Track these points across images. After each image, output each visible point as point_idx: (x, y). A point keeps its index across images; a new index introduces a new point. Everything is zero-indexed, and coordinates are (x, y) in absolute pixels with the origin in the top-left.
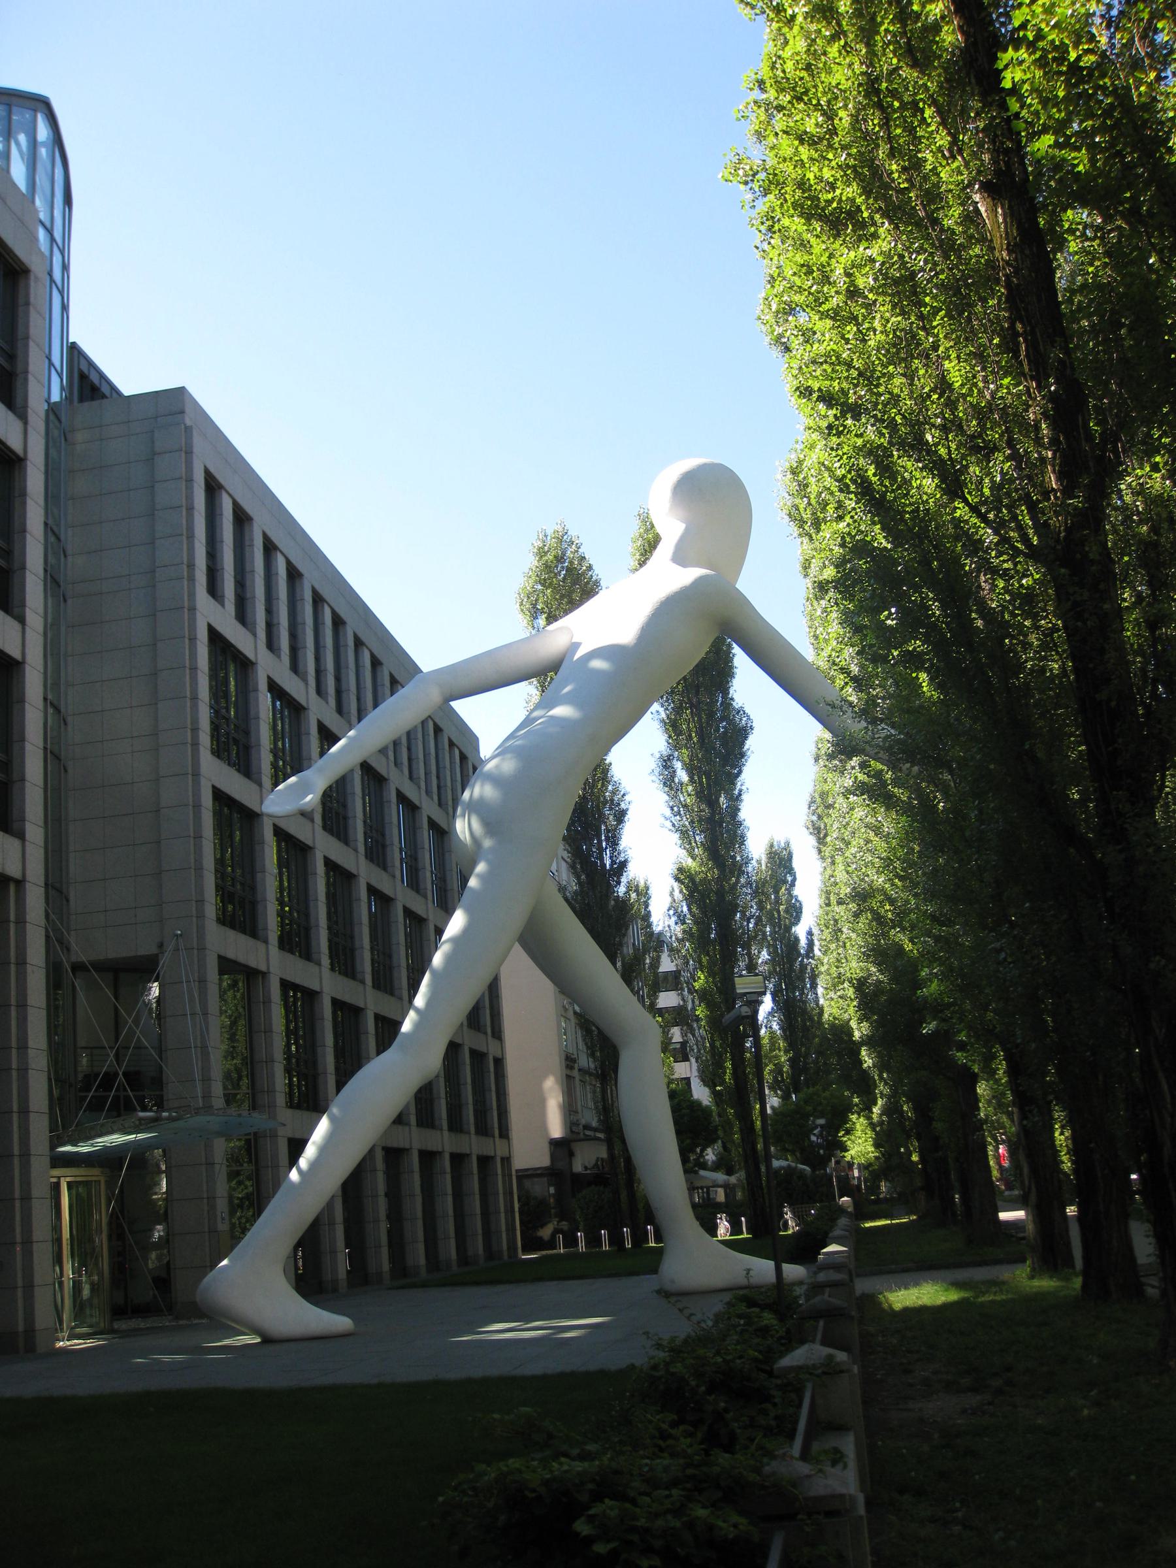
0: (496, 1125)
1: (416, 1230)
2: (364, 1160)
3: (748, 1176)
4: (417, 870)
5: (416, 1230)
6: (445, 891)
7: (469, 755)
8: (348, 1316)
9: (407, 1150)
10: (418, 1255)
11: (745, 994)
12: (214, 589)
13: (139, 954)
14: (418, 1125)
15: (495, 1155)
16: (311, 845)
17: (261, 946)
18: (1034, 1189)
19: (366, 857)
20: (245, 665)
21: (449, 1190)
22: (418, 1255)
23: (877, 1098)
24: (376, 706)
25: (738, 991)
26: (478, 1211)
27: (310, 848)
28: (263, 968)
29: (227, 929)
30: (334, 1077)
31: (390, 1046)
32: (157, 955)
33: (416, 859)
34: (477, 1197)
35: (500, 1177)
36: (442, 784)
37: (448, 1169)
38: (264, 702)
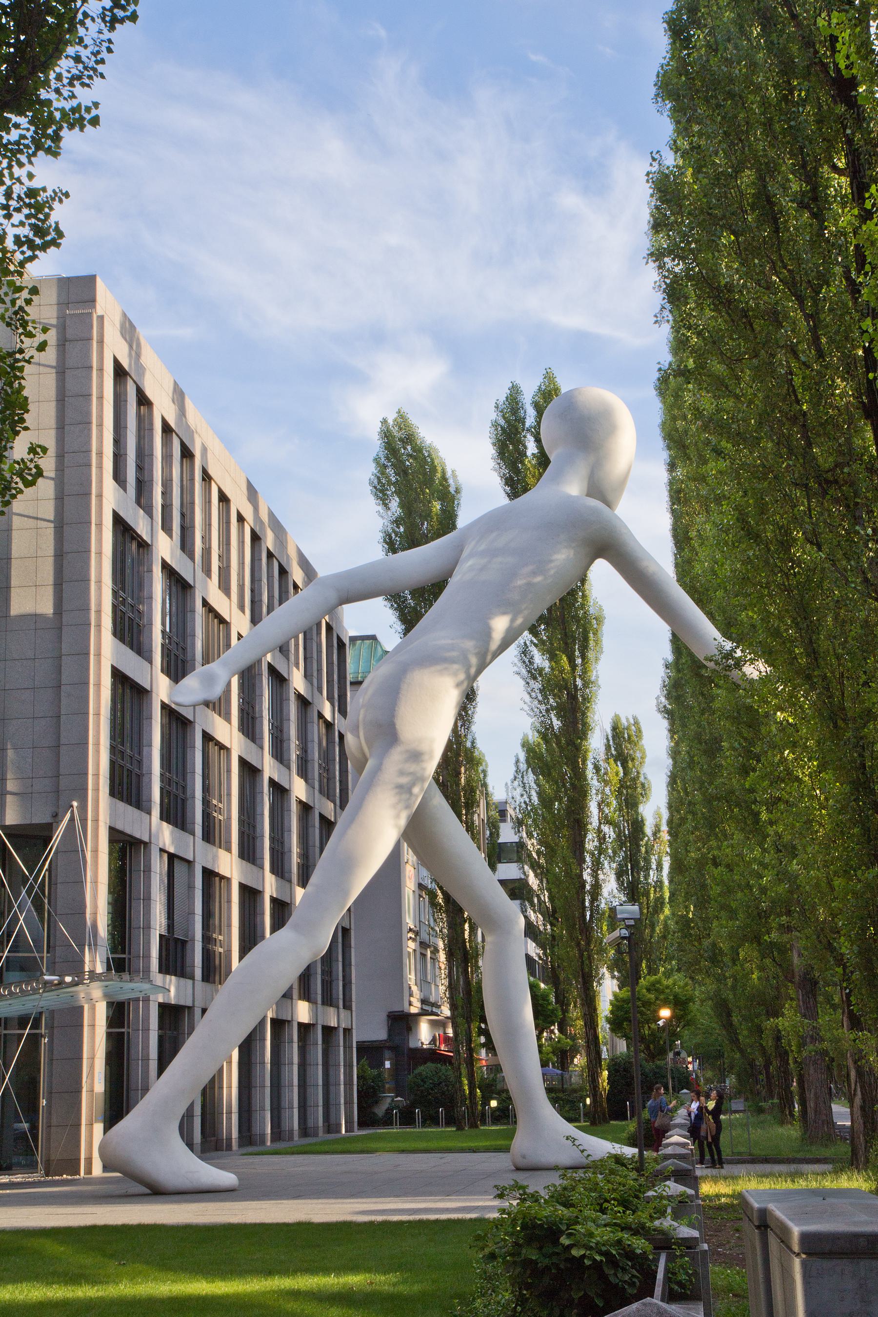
0: (341, 996)
1: (264, 1097)
2: (255, 1029)
3: (590, 1061)
4: (282, 741)
5: (264, 1097)
6: (306, 761)
7: (334, 626)
8: (235, 1173)
9: (289, 1021)
10: (231, 1125)
11: (624, 920)
12: (119, 477)
13: (33, 822)
14: (203, 980)
15: (339, 1027)
16: (149, 689)
17: (145, 816)
18: (859, 1089)
19: (115, 634)
20: (144, 546)
21: (296, 1060)
22: (231, 1125)
23: (727, 635)
24: (280, 604)
25: (619, 916)
26: (320, 1082)
27: (190, 722)
28: (146, 838)
29: (117, 801)
30: (201, 944)
31: (283, 926)
32: (51, 824)
33: (281, 731)
34: (320, 1067)
35: (342, 1049)
36: (308, 656)
37: (320, 1041)
38: (158, 584)
